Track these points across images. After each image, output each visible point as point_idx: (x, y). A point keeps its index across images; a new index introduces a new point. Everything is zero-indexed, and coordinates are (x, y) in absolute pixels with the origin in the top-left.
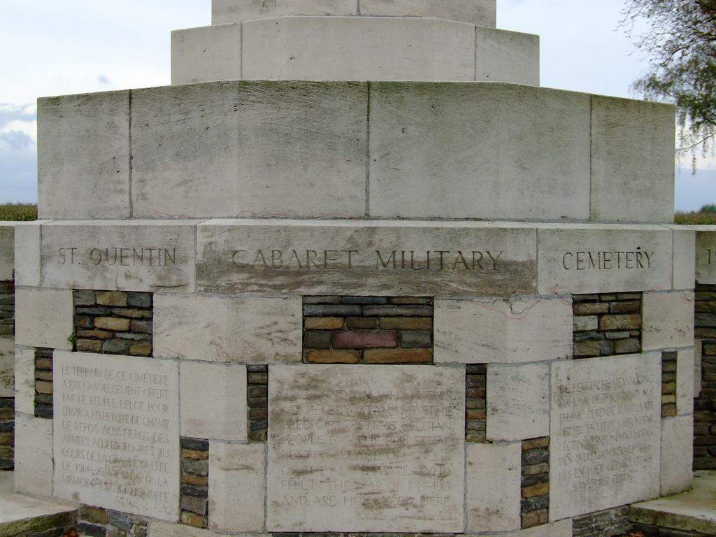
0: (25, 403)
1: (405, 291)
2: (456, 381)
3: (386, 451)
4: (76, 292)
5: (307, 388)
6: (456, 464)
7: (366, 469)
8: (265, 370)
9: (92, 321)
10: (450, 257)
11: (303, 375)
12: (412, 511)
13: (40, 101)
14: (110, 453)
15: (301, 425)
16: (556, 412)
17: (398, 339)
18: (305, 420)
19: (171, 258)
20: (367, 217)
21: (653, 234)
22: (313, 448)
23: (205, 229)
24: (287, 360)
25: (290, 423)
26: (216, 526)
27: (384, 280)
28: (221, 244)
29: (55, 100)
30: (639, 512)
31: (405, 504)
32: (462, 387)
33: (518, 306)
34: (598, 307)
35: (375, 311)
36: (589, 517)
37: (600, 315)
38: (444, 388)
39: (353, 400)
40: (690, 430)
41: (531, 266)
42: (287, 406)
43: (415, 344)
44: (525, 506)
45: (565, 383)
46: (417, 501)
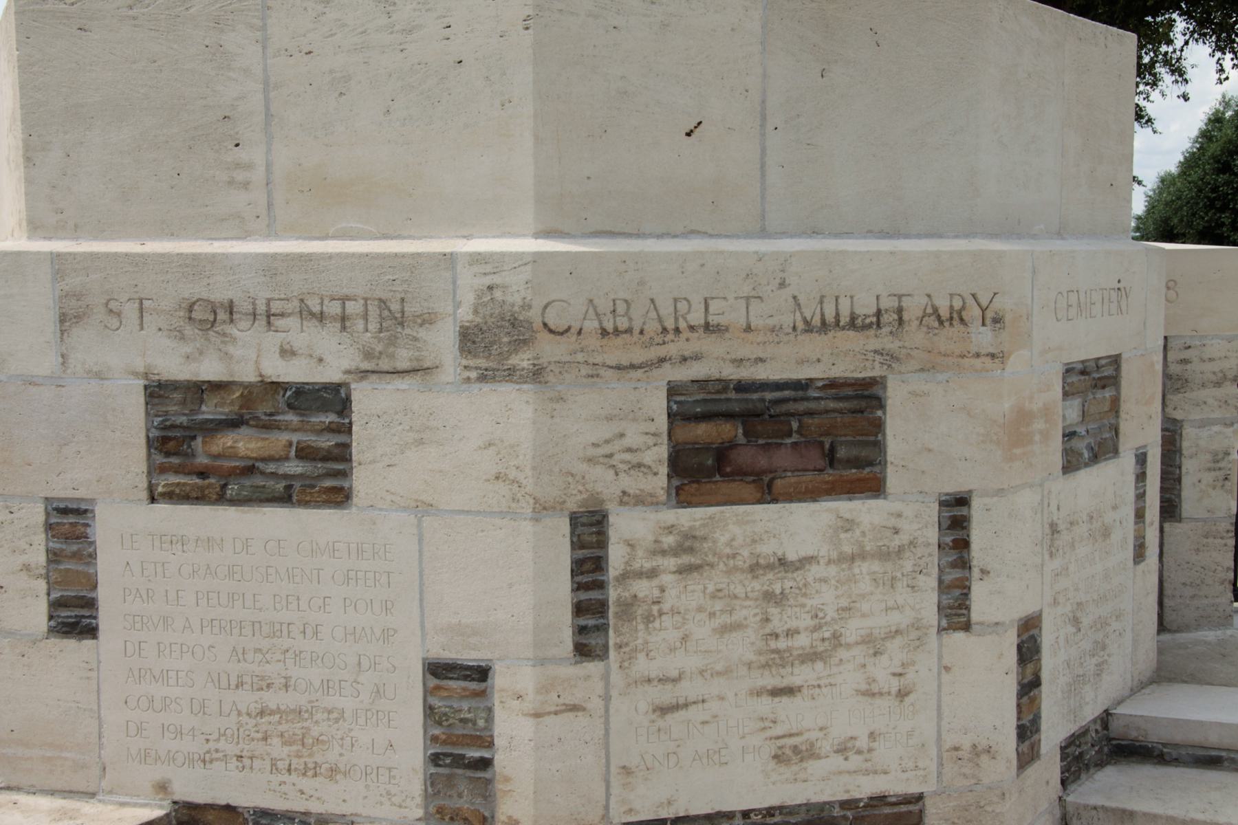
3: (811, 657)
5: (677, 551)
7: (776, 692)
11: (670, 529)
12: (855, 761)
14: (247, 699)
18: (675, 612)
22: (691, 662)
23: (477, 259)
24: (640, 500)
25: (649, 619)
31: (842, 750)
38: (904, 538)
39: (755, 569)
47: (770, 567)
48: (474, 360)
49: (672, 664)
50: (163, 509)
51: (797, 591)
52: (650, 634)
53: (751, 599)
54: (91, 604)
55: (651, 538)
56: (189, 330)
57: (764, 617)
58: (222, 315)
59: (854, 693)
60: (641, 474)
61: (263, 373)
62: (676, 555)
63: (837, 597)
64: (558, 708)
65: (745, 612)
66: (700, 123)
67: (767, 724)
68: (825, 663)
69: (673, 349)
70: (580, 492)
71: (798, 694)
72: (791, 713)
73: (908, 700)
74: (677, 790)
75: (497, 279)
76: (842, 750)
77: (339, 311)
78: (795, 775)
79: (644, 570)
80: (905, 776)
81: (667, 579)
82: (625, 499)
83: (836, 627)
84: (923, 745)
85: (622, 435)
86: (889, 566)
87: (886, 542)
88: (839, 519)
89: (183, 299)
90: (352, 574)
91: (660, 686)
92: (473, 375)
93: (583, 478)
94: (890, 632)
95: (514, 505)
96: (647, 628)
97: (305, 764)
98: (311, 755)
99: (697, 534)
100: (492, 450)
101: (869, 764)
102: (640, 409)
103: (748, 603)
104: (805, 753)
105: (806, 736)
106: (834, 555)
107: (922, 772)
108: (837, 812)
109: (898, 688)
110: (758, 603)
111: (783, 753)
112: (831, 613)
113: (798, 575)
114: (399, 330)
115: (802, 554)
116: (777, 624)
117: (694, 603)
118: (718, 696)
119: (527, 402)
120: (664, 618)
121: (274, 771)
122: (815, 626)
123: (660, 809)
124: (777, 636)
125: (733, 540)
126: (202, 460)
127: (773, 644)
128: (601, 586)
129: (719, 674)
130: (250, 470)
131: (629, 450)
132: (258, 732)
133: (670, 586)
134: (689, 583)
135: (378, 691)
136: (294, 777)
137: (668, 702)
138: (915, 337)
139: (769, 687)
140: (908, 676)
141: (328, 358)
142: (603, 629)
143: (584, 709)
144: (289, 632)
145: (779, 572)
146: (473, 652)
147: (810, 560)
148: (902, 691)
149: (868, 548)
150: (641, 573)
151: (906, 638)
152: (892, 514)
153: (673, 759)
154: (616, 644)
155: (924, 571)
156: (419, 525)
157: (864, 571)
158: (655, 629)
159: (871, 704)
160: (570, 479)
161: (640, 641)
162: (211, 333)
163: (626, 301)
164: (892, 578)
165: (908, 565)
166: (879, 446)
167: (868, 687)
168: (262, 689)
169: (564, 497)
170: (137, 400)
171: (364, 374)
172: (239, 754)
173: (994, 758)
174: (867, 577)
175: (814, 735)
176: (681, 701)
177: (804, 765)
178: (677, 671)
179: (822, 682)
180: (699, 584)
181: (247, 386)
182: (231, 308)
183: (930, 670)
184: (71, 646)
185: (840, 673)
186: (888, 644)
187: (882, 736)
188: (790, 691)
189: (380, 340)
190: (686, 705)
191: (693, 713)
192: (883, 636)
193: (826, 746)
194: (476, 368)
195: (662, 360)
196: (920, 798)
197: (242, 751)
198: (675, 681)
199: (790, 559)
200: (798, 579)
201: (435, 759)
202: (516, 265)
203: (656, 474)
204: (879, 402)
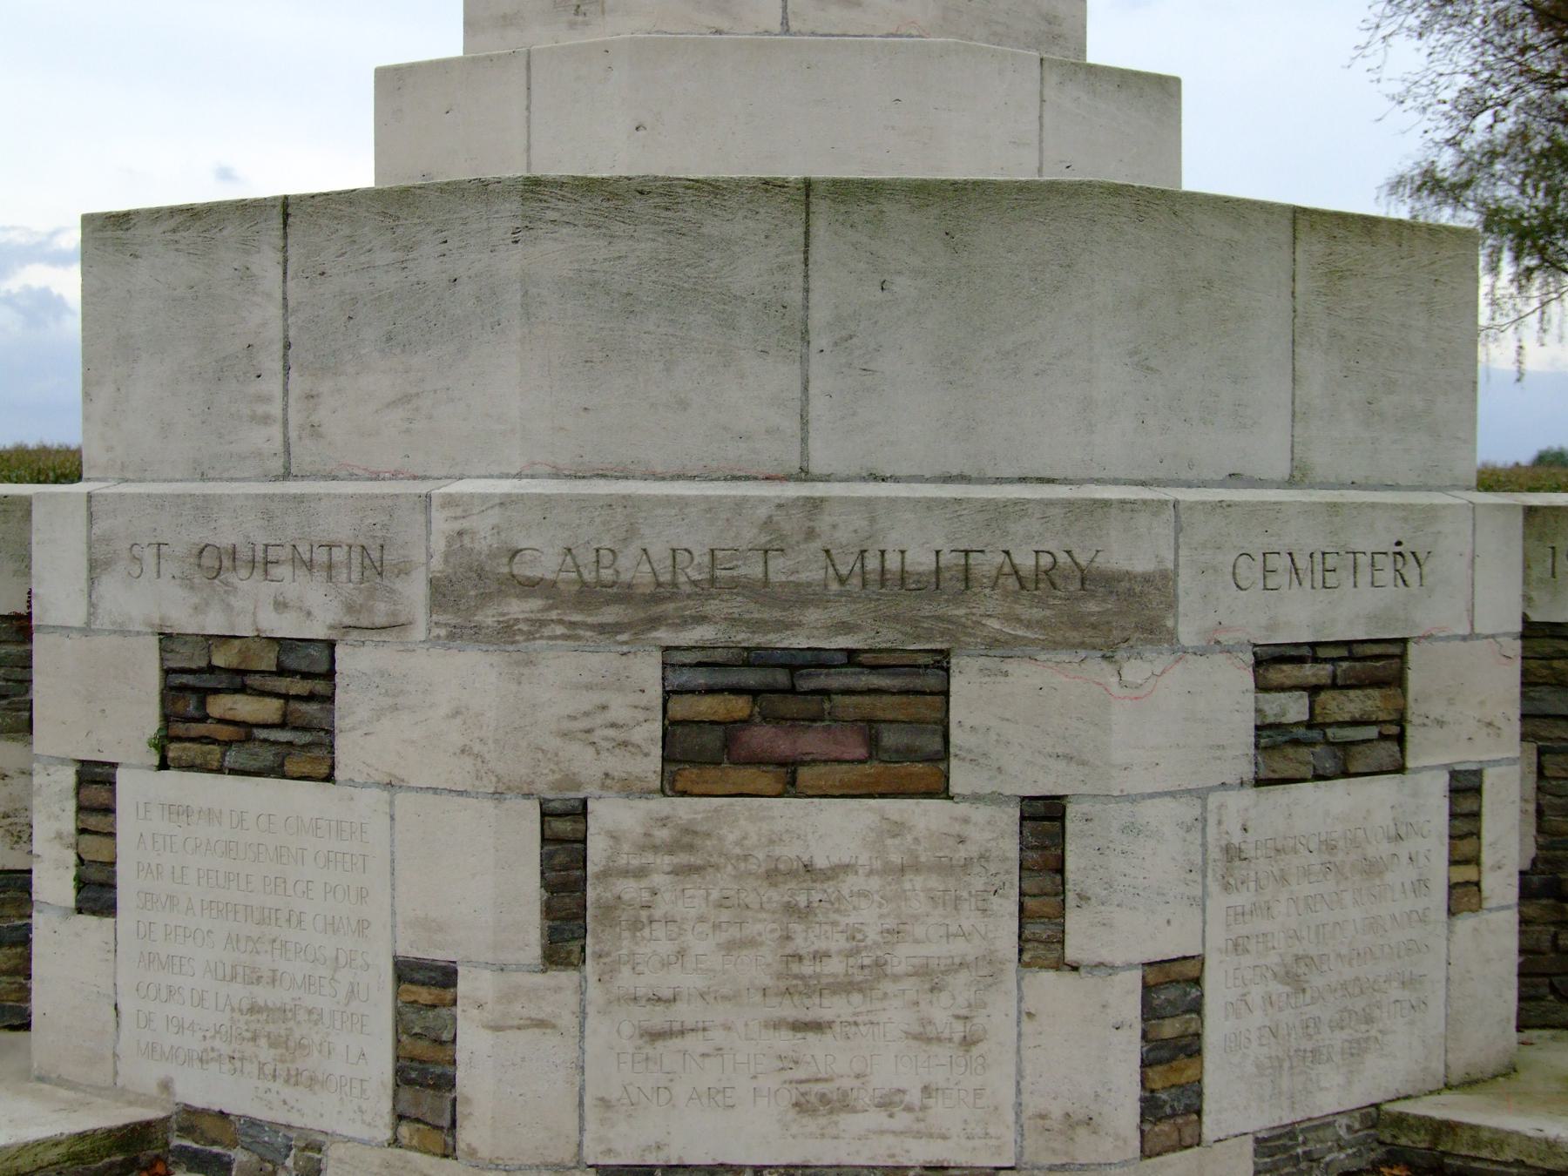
1: (888, 637)
3: (845, 987)
4: (167, 639)
5: (671, 848)
6: (999, 1016)
8: (580, 811)
9: (202, 704)
10: (986, 564)
11: (664, 822)
12: (902, 1120)
13: (89, 221)
15: (660, 930)
16: (1218, 902)
17: (873, 742)
18: (669, 920)
20: (804, 475)
21: (1431, 512)
22: (686, 980)
23: (450, 501)
24: (629, 789)
25: (636, 926)
26: (472, 1152)
27: (842, 612)
28: (484, 532)
29: (121, 220)
30: (1400, 1121)
31: (886, 1104)
32: (1011, 848)
33: (1135, 670)
34: (1310, 673)
35: (822, 680)
36: (1289, 1132)
37: (1314, 690)
38: (972, 850)
39: (773, 875)
40: (1512, 942)
41: (1162, 583)
42: (629, 889)
43: (908, 754)
44: (1151, 1108)
47: (792, 874)
48: (445, 616)
49: (666, 981)
51: (829, 906)
52: (637, 944)
53: (768, 911)
55: (640, 830)
57: (785, 933)
58: (227, 563)
59: (904, 1035)
60: (628, 754)
61: (260, 627)
62: (671, 853)
63: (881, 916)
64: (521, 1022)
65: (759, 927)
67: (787, 1064)
68: (864, 996)
70: (553, 772)
71: (828, 1031)
72: (820, 1053)
73: (975, 1051)
74: (669, 1133)
75: (465, 524)
76: (886, 1104)
77: (325, 558)
78: (823, 1128)
79: (631, 867)
80: (970, 1144)
81: (658, 879)
83: (879, 953)
84: (996, 1108)
85: (604, 708)
86: (951, 883)
87: (946, 852)
88: (884, 821)
89: (194, 544)
90: (332, 855)
91: (649, 1007)
92: (443, 632)
93: (557, 755)
94: (953, 964)
95: (477, 783)
96: (634, 936)
97: (288, 1070)
98: (293, 1061)
99: (699, 828)
100: (458, 720)
101: (922, 1125)
102: (628, 677)
103: (764, 915)
105: (837, 1084)
106: (878, 864)
107: (993, 1142)
109: (962, 1034)
110: (777, 916)
111: (808, 1102)
112: (872, 935)
113: (830, 886)
114: (378, 580)
115: (835, 860)
116: (800, 944)
117: (693, 912)
118: (723, 1025)
119: (491, 665)
120: (655, 925)
121: (262, 1076)
122: (852, 950)
123: (646, 1153)
124: (800, 958)
125: (745, 838)
127: (795, 968)
129: (725, 998)
131: (613, 725)
132: (247, 1030)
133: (663, 889)
134: (689, 886)
135: (353, 991)
136: (277, 1085)
137: (658, 1027)
139: (790, 1020)
140: (975, 1021)
141: (315, 611)
143: (554, 1027)
144: (277, 919)
145: (804, 881)
146: (438, 951)
147: (846, 868)
148: (968, 1038)
149: (923, 859)
150: (627, 872)
151: (974, 974)
152: (956, 819)
153: (664, 1095)
154: (594, 953)
155: (1000, 891)
156: (392, 803)
157: (918, 887)
158: (643, 938)
159: (925, 1051)
160: (540, 755)
161: (624, 951)
162: (216, 581)
163: (612, 551)
164: (956, 896)
167: (922, 1030)
168: (252, 983)
169: (533, 776)
172: (232, 1054)
173: (1094, 1133)
174: (921, 894)
175: (846, 1083)
176: (677, 1026)
177: (834, 1118)
178: (671, 991)
179: (860, 1019)
180: (700, 888)
183: (1007, 1015)
185: (884, 1009)
186: (949, 979)
187: (940, 1092)
188: (817, 1027)
189: (361, 592)
190: (682, 1033)
191: (693, 1043)
192: (943, 968)
194: (446, 625)
197: (234, 1052)
199: (818, 866)
200: (830, 891)
202: (484, 508)
203: (646, 755)
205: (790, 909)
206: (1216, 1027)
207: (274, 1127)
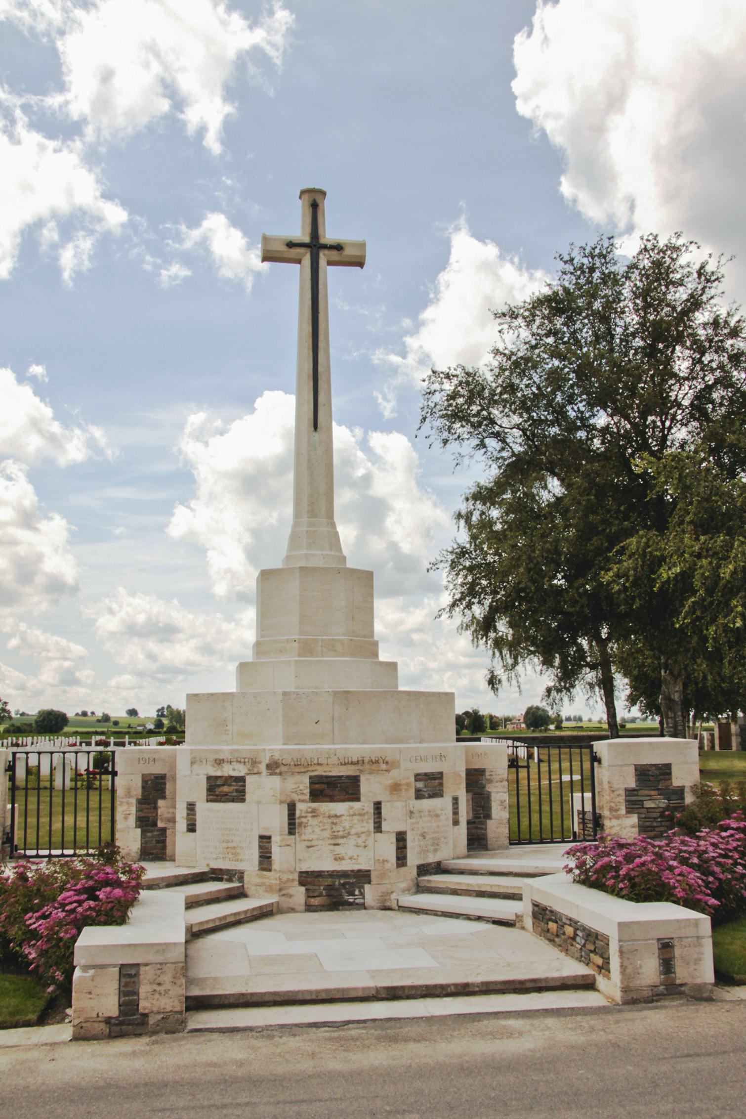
0: (181, 825)
2: (370, 809)
3: (343, 837)
5: (312, 812)
6: (370, 842)
7: (335, 845)
11: (310, 807)
12: (354, 861)
13: (188, 695)
14: (225, 845)
15: (309, 827)
18: (311, 825)
19: (254, 762)
23: (270, 750)
24: (303, 801)
25: (305, 827)
26: (275, 870)
29: (196, 695)
31: (350, 858)
36: (423, 865)
38: (365, 811)
39: (330, 817)
40: (465, 831)
42: (303, 820)
44: (398, 858)
45: (412, 809)
46: (355, 857)
50: (210, 804)
54: (195, 825)
56: (216, 765)
66: (316, 427)
69: (311, 768)
72: (338, 849)
76: (350, 858)
82: (300, 801)
104: (342, 859)
108: (350, 873)
126: (217, 793)
128: (295, 819)
130: (226, 795)
138: (367, 766)
142: (295, 829)
147: (341, 816)
165: (366, 817)
166: (359, 791)
170: (205, 780)
171: (248, 774)
181: (226, 777)
182: (223, 760)
184: (190, 834)
188: (338, 844)
191: (315, 848)
193: (346, 857)
195: (308, 771)
196: (369, 871)
198: (311, 841)
201: (261, 857)
204: (359, 781)
205: (333, 823)
206: (409, 844)
207: (232, 870)
